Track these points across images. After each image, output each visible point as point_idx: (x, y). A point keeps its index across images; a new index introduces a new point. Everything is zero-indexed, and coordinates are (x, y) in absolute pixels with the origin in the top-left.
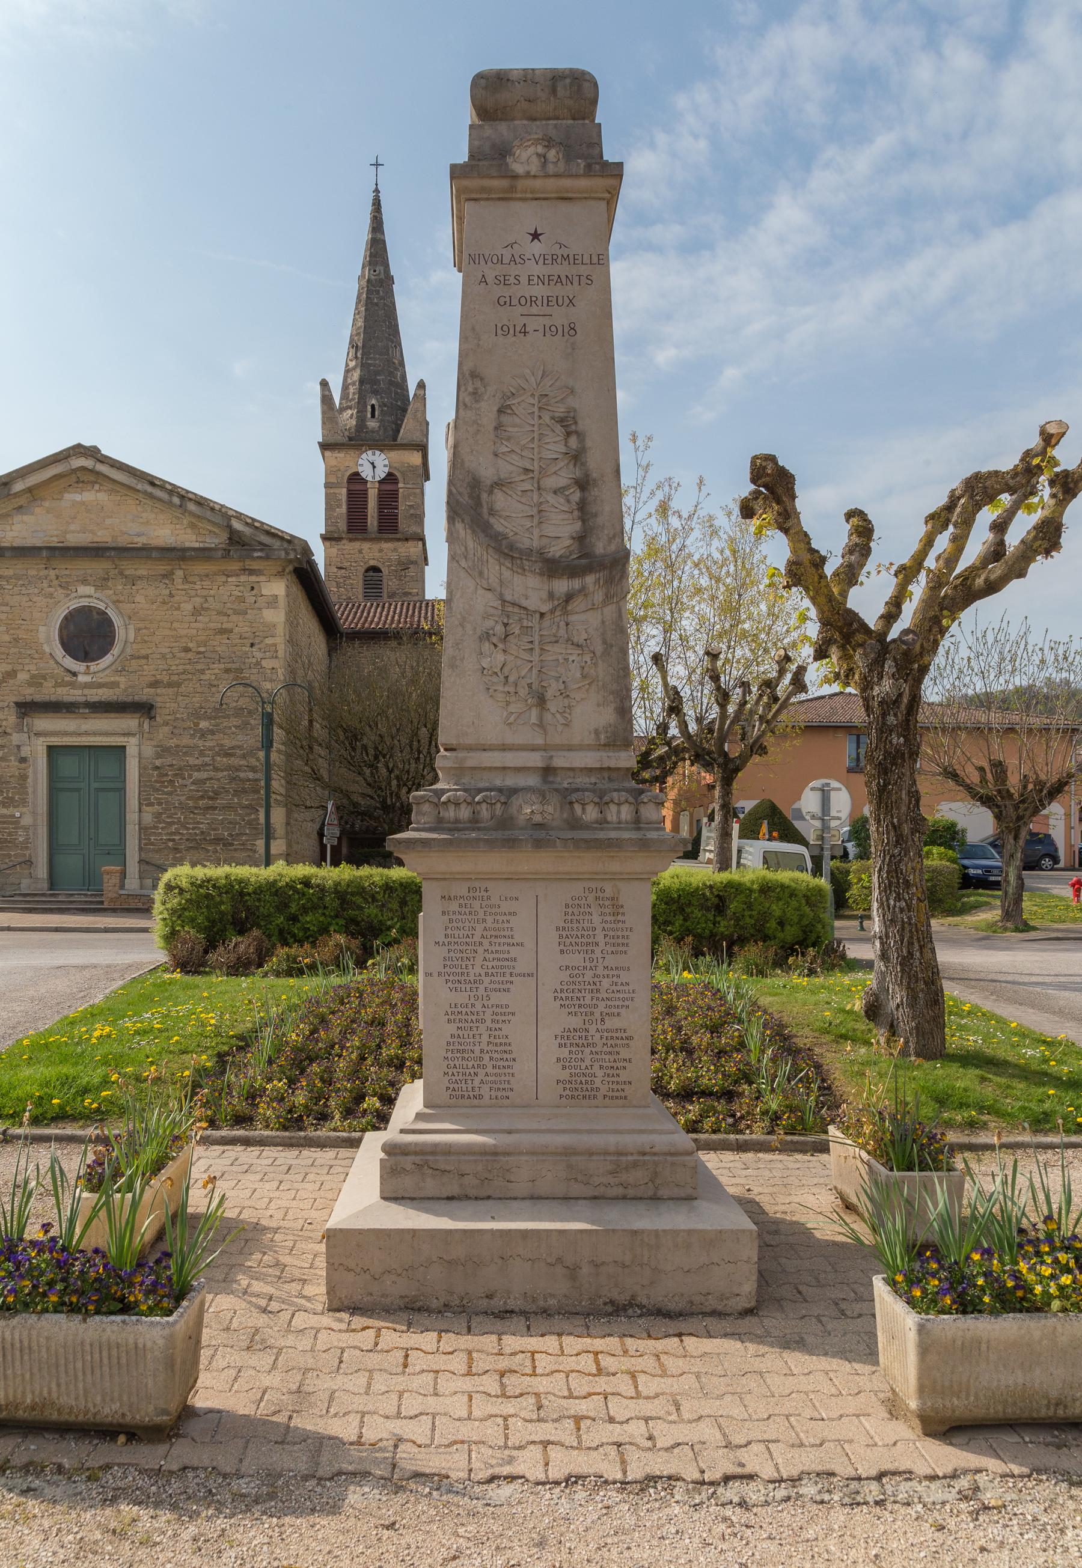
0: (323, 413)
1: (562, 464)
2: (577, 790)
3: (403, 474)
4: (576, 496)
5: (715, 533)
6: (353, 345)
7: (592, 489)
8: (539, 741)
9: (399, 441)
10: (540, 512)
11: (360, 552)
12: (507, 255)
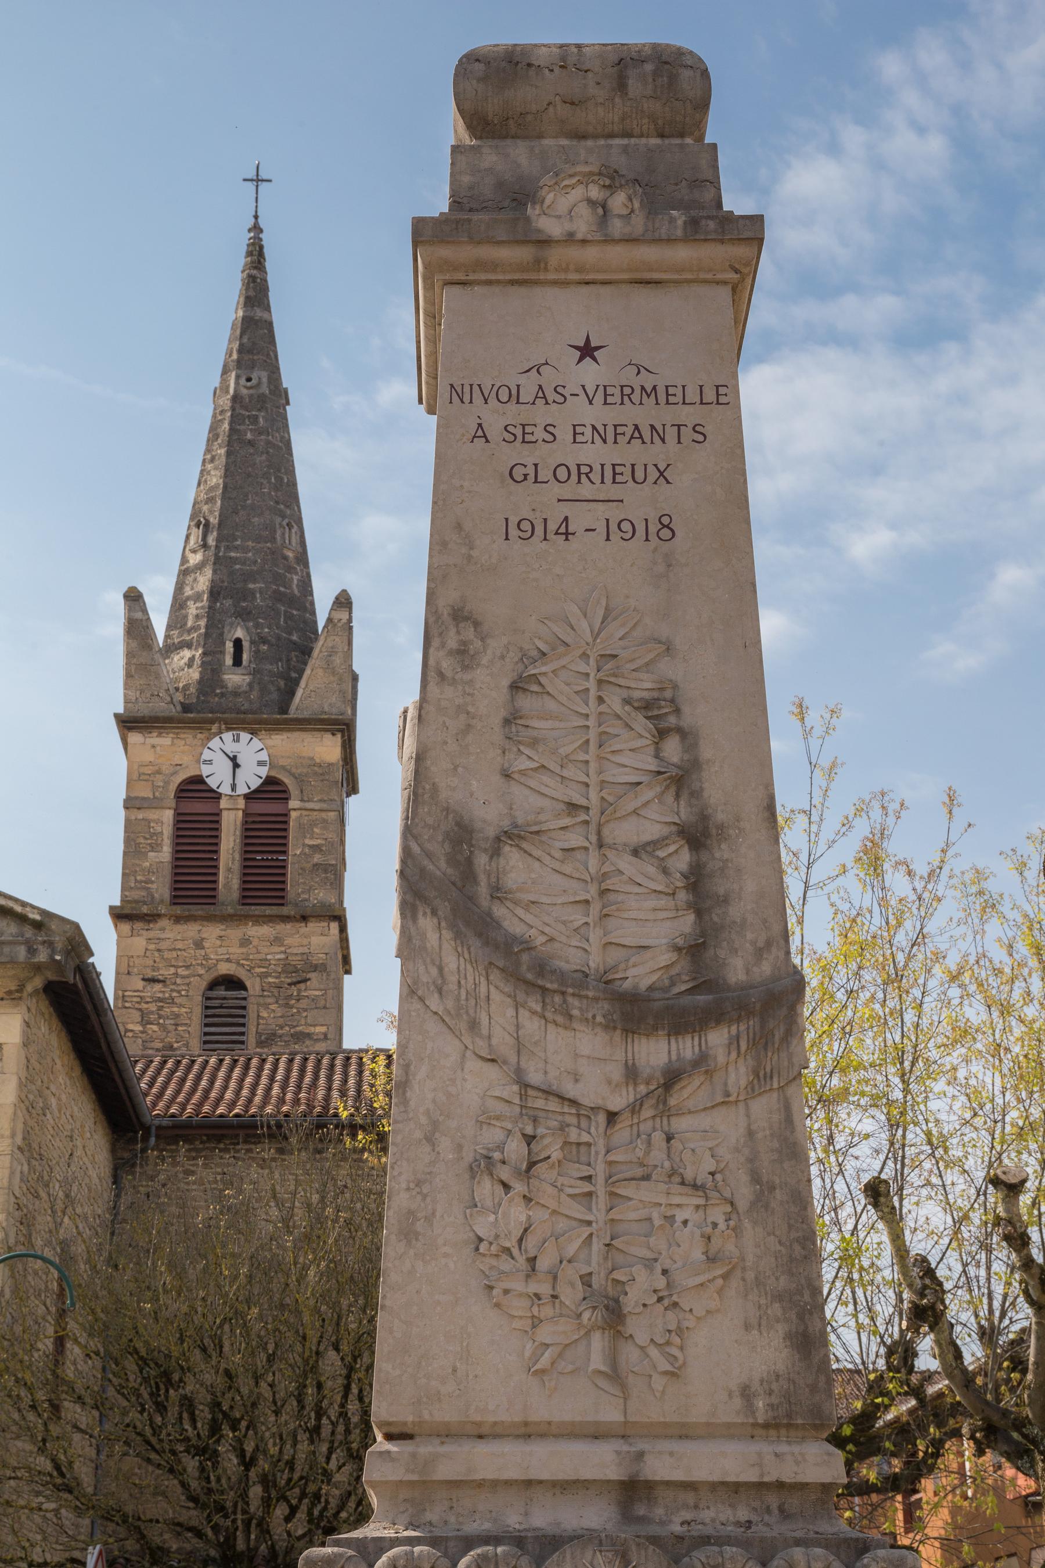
0: (129, 655)
1: (648, 794)
2: (705, 1541)
3: (299, 779)
4: (682, 860)
5: (990, 906)
6: (199, 521)
7: (713, 843)
8: (611, 1414)
9: (293, 713)
10: (603, 893)
11: (199, 944)
12: (528, 388)
